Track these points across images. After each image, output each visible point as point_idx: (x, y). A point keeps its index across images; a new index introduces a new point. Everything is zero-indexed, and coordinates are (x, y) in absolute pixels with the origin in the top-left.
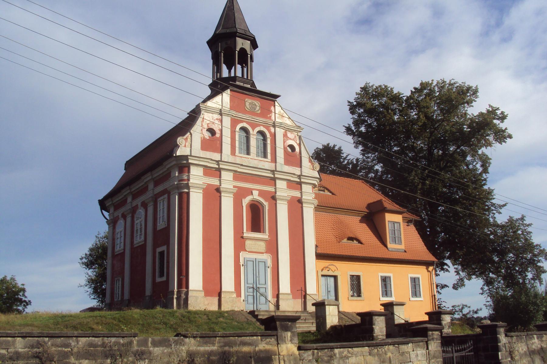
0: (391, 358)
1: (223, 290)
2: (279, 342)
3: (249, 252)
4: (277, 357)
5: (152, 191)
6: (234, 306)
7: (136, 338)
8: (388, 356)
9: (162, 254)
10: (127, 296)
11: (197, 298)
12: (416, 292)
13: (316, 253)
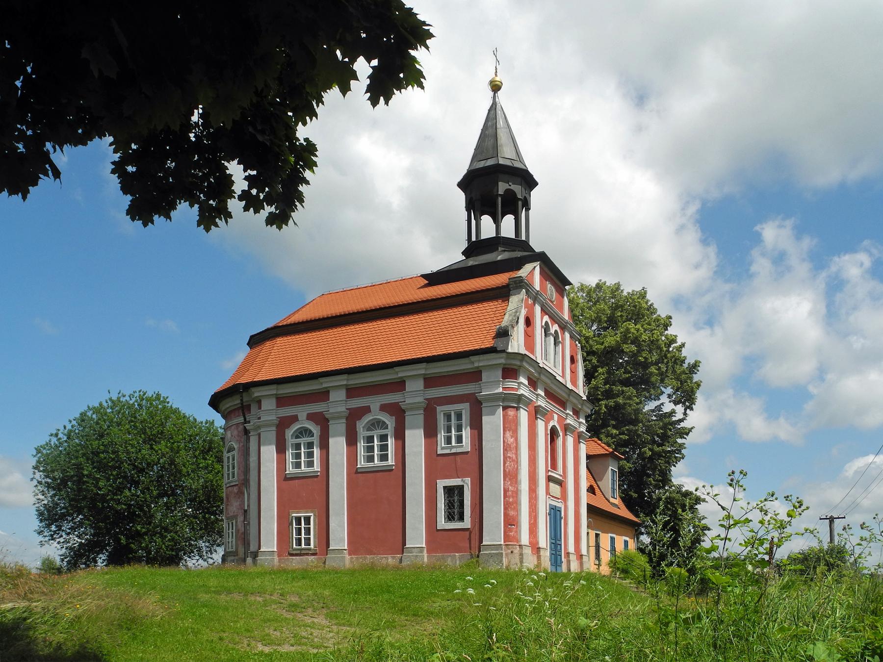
13: (587, 503)
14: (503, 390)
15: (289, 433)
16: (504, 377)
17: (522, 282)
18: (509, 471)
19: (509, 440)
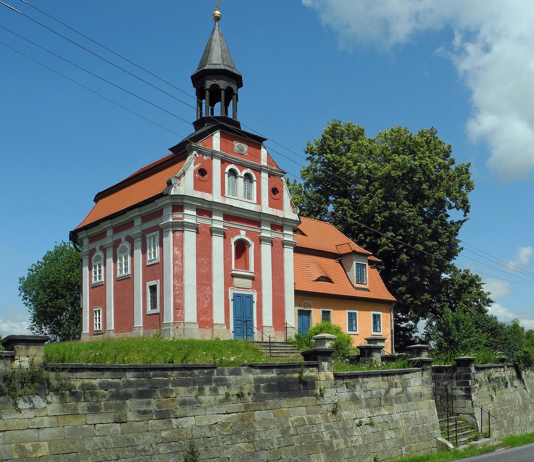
6: (225, 336)
13: (295, 290)
14: (173, 220)
17: (192, 147)
18: (176, 273)
19: (176, 253)
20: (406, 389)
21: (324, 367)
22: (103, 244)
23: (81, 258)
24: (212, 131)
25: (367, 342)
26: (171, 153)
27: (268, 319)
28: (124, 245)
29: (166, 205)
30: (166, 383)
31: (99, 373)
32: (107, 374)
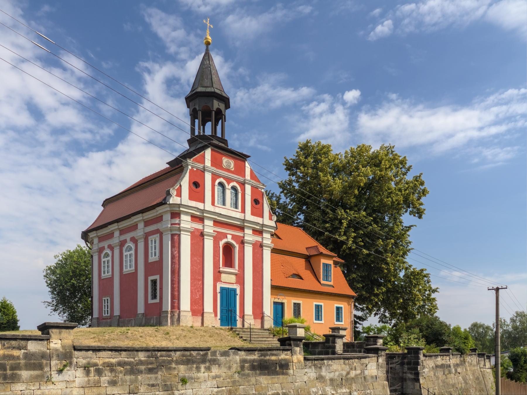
0: (356, 367)
1: (205, 311)
2: (293, 354)
3: (224, 282)
4: (292, 363)
5: (142, 229)
6: (213, 323)
7: (210, 351)
8: (354, 365)
9: (154, 282)
10: (117, 312)
11: (186, 316)
12: (318, 317)
13: (271, 285)
15: (124, 249)
16: (172, 218)
20: (364, 372)
21: (296, 351)
22: (111, 243)
23: (92, 254)
24: (204, 148)
25: (331, 330)
26: (168, 166)
27: (249, 309)
28: (129, 245)
29: (166, 212)
30: (170, 362)
31: (117, 353)
32: (124, 353)
